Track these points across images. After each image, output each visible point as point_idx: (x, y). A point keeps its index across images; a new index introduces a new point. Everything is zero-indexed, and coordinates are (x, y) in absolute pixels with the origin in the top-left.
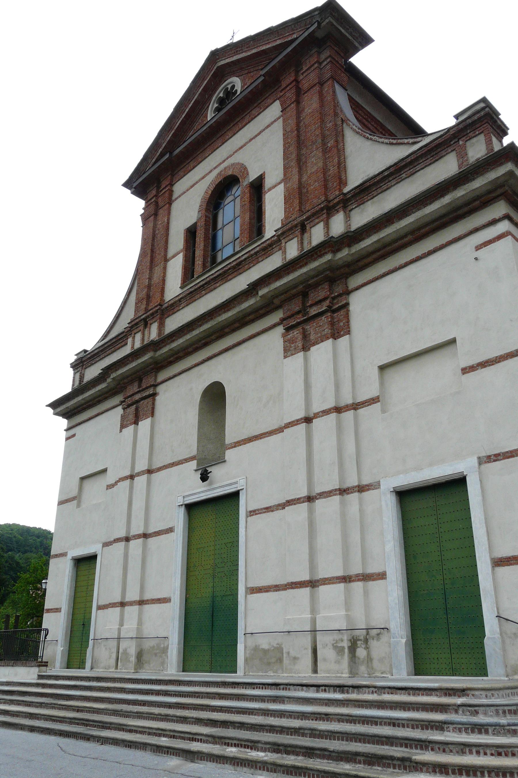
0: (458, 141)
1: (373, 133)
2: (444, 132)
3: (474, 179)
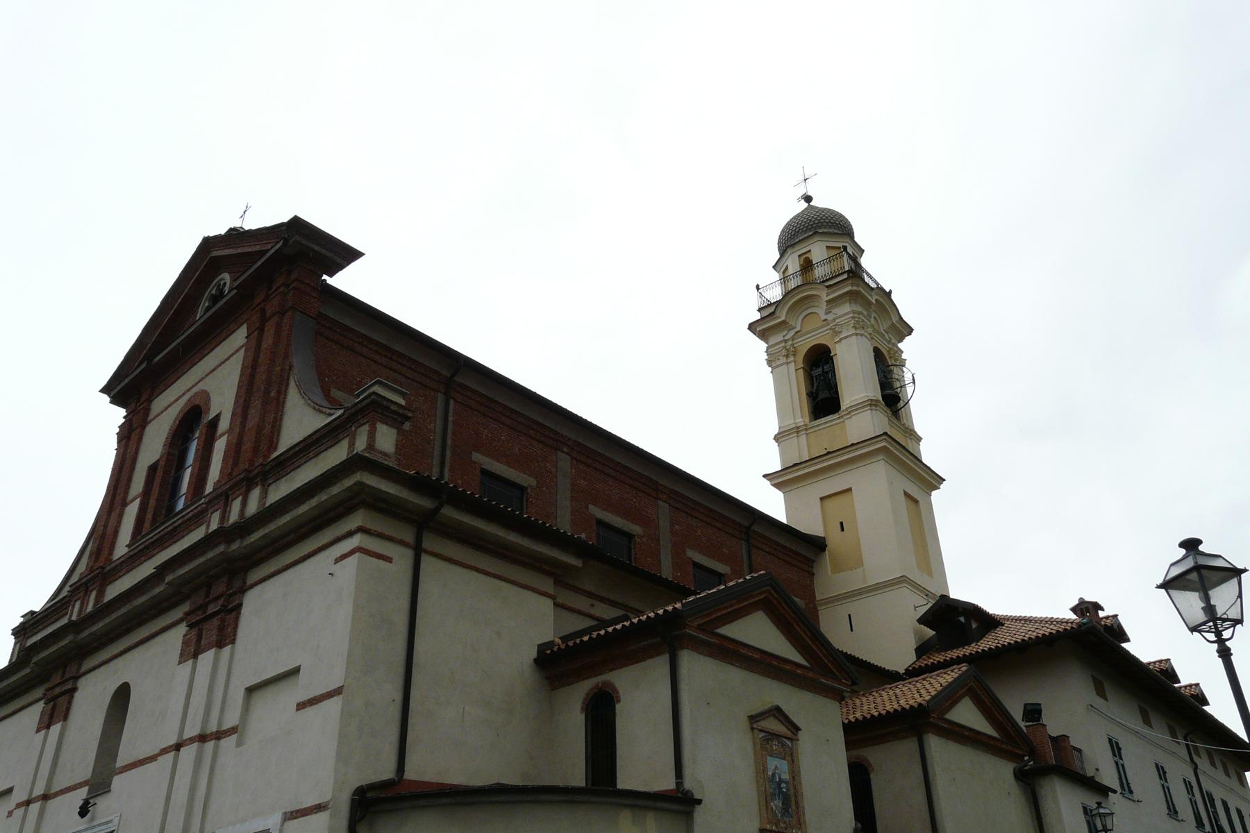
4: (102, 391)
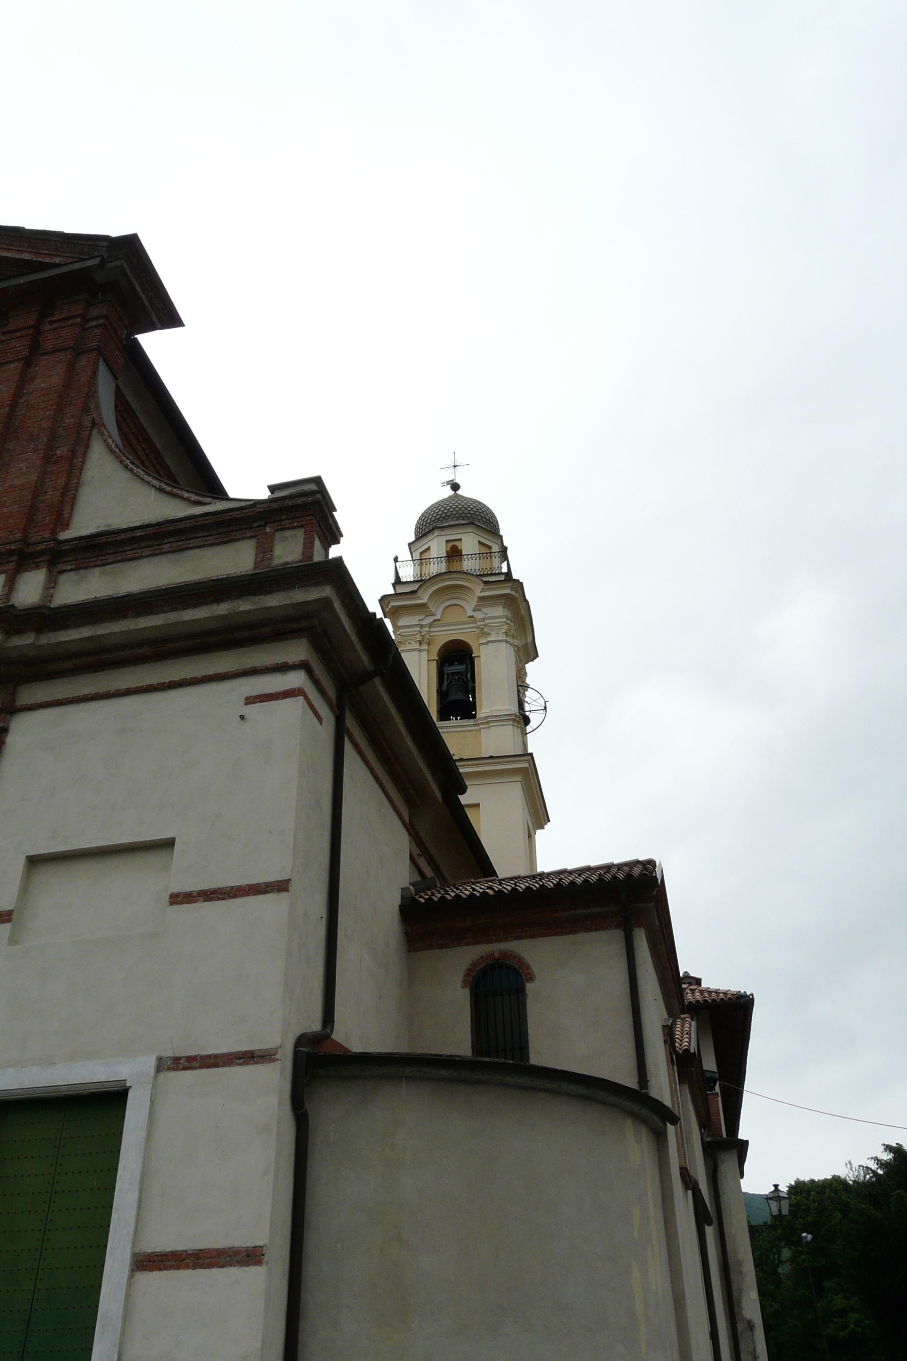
0: (265, 526)
1: (143, 465)
2: (248, 503)
3: (271, 592)
4: (183, 325)
